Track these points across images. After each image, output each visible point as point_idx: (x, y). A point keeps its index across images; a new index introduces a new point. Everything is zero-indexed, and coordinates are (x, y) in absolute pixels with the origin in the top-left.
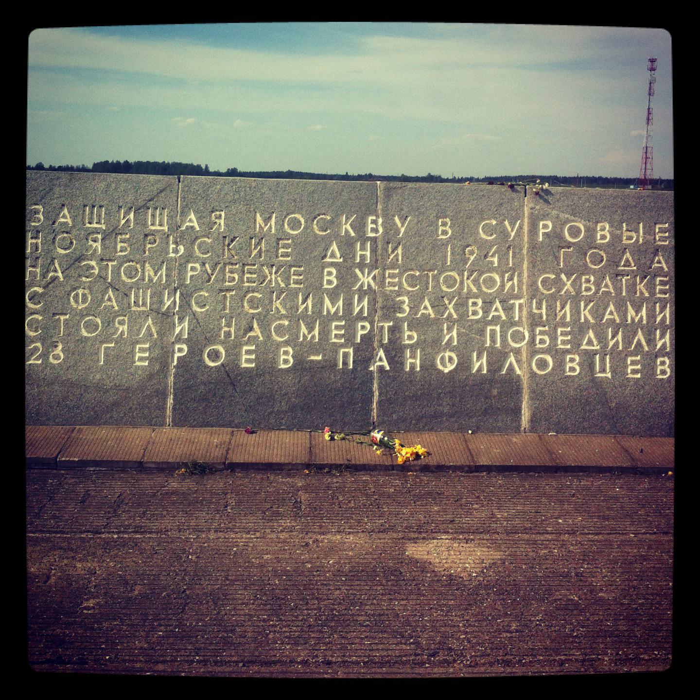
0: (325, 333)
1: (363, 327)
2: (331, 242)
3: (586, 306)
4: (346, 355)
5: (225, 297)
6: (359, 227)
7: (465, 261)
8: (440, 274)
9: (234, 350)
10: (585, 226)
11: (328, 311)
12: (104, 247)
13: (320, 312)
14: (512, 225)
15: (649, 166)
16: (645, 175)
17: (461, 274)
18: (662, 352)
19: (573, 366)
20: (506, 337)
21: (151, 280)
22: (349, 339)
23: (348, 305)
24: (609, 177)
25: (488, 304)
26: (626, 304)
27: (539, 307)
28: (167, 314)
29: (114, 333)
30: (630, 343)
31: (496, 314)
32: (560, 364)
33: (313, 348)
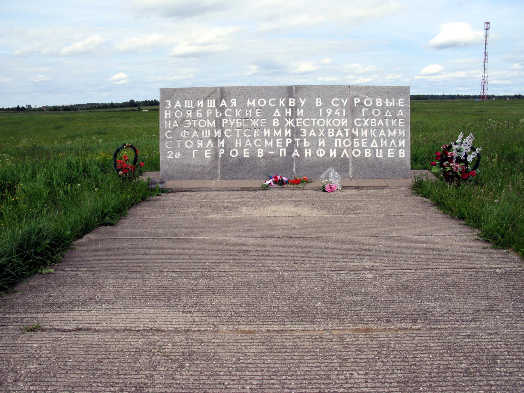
0: (275, 143)
4: (283, 151)
9: (241, 150)
14: (345, 100)
18: (402, 147)
23: (283, 133)
25: (336, 131)
28: (217, 138)
32: (363, 153)
33: (271, 149)
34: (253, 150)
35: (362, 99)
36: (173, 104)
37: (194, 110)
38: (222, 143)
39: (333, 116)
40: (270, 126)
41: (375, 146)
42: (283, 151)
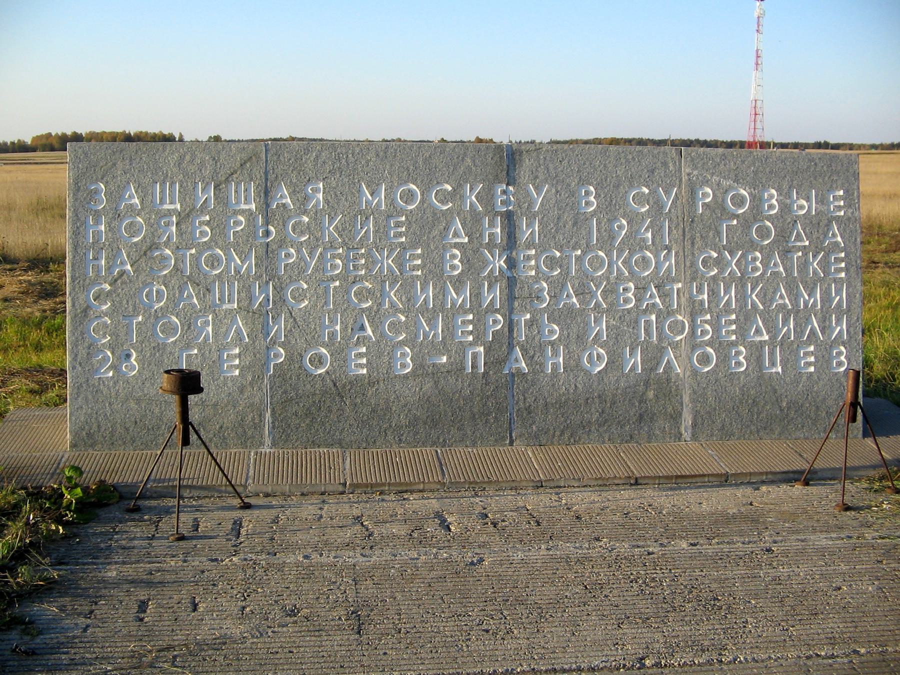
0: (449, 330)
1: (495, 322)
2: (453, 218)
3: (753, 289)
4: (475, 356)
5: (327, 289)
6: (486, 198)
7: (612, 238)
8: (584, 253)
9: (340, 353)
10: (750, 194)
11: (453, 304)
12: (180, 232)
13: (443, 304)
14: (667, 192)
15: (759, 125)
16: (754, 136)
17: (609, 254)
18: (838, 341)
19: (741, 360)
20: (663, 329)
21: (237, 272)
22: (479, 338)
23: (477, 295)
24: (708, 140)
25: (641, 290)
26: (798, 287)
27: (700, 290)
28: (262, 313)
29: (197, 338)
30: (803, 332)
31: (781, 302)
32: (724, 358)
33: (437, 348)
34: (381, 352)
35: (721, 192)
36: (115, 196)
37: (184, 217)
38: (279, 327)
39: (634, 243)
40: (435, 271)
41: (758, 339)
42: (475, 356)
